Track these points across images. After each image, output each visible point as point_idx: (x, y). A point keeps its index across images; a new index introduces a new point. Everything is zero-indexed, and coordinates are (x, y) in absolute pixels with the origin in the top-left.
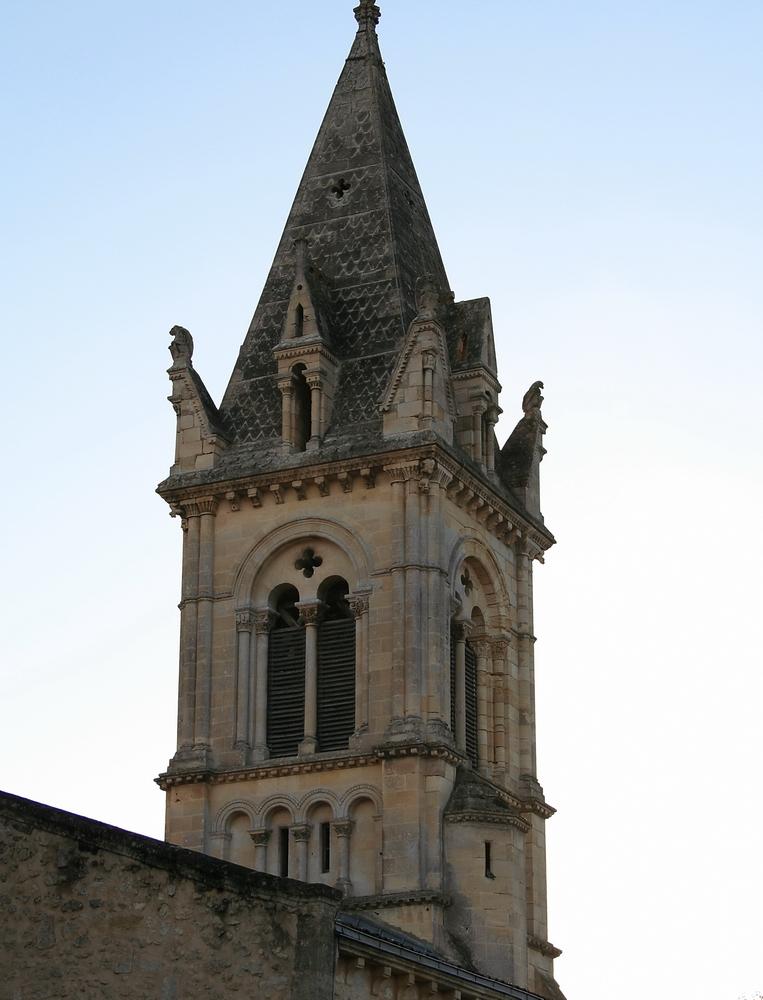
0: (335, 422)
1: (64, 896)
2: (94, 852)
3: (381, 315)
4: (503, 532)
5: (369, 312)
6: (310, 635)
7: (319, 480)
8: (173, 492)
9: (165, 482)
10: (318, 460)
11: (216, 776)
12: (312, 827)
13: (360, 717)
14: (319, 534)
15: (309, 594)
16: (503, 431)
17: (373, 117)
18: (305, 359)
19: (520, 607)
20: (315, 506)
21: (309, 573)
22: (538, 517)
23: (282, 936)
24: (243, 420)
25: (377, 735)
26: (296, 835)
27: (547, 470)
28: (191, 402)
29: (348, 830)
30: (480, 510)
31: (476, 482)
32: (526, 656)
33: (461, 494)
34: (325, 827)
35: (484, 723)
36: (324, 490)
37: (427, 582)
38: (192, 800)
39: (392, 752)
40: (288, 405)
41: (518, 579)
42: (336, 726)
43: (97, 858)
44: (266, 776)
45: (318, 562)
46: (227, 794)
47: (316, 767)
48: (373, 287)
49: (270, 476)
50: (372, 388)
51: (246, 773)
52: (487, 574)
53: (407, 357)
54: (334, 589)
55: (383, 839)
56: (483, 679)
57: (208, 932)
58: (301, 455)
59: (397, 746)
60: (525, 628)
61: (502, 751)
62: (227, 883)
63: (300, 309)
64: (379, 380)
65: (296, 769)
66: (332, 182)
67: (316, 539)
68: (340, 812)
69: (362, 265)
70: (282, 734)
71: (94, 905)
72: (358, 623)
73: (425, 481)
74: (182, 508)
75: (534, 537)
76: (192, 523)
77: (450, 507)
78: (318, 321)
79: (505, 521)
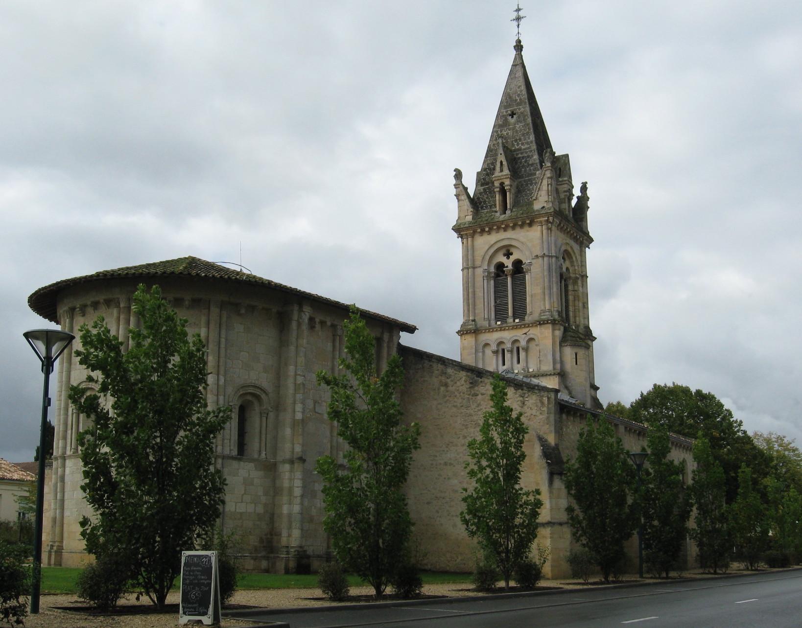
0: (516, 204)
1: (472, 391)
2: (481, 378)
3: (530, 163)
4: (576, 240)
5: (526, 162)
6: (509, 280)
7: (511, 225)
8: (459, 229)
9: (455, 226)
10: (510, 218)
11: (479, 330)
12: (513, 348)
13: (529, 309)
14: (512, 244)
15: (509, 263)
16: (574, 202)
17: (523, 88)
18: (504, 181)
19: (582, 266)
20: (510, 234)
21: (508, 258)
22: (587, 232)
23: (542, 403)
24: (481, 202)
25: (536, 316)
26: (508, 351)
27: (590, 214)
28: (463, 196)
29: (526, 350)
30: (568, 233)
31: (567, 223)
32: (585, 283)
33: (562, 228)
34: (518, 349)
35: (571, 308)
36: (513, 228)
37: (552, 261)
38: (470, 339)
39: (542, 322)
40: (498, 197)
41: (581, 255)
42: (520, 311)
43: (482, 380)
44: (496, 331)
45: (512, 254)
46: (485, 337)
47: (516, 327)
48: (526, 153)
49: (493, 224)
50: (529, 190)
51: (489, 329)
52: (570, 255)
53: (542, 180)
54: (518, 264)
55: (540, 352)
56: (570, 293)
57: (519, 402)
58: (503, 216)
59: (544, 321)
60: (584, 273)
61: (577, 318)
62: (525, 388)
63: (501, 162)
64: (531, 187)
65: (507, 328)
66: (509, 112)
67: (511, 246)
68: (523, 343)
69: (522, 144)
70: (500, 313)
71: (482, 394)
72: (527, 276)
73: (550, 225)
74: (461, 235)
75: (586, 240)
76: (465, 240)
77: (558, 233)
78: (508, 166)
79: (577, 236)
